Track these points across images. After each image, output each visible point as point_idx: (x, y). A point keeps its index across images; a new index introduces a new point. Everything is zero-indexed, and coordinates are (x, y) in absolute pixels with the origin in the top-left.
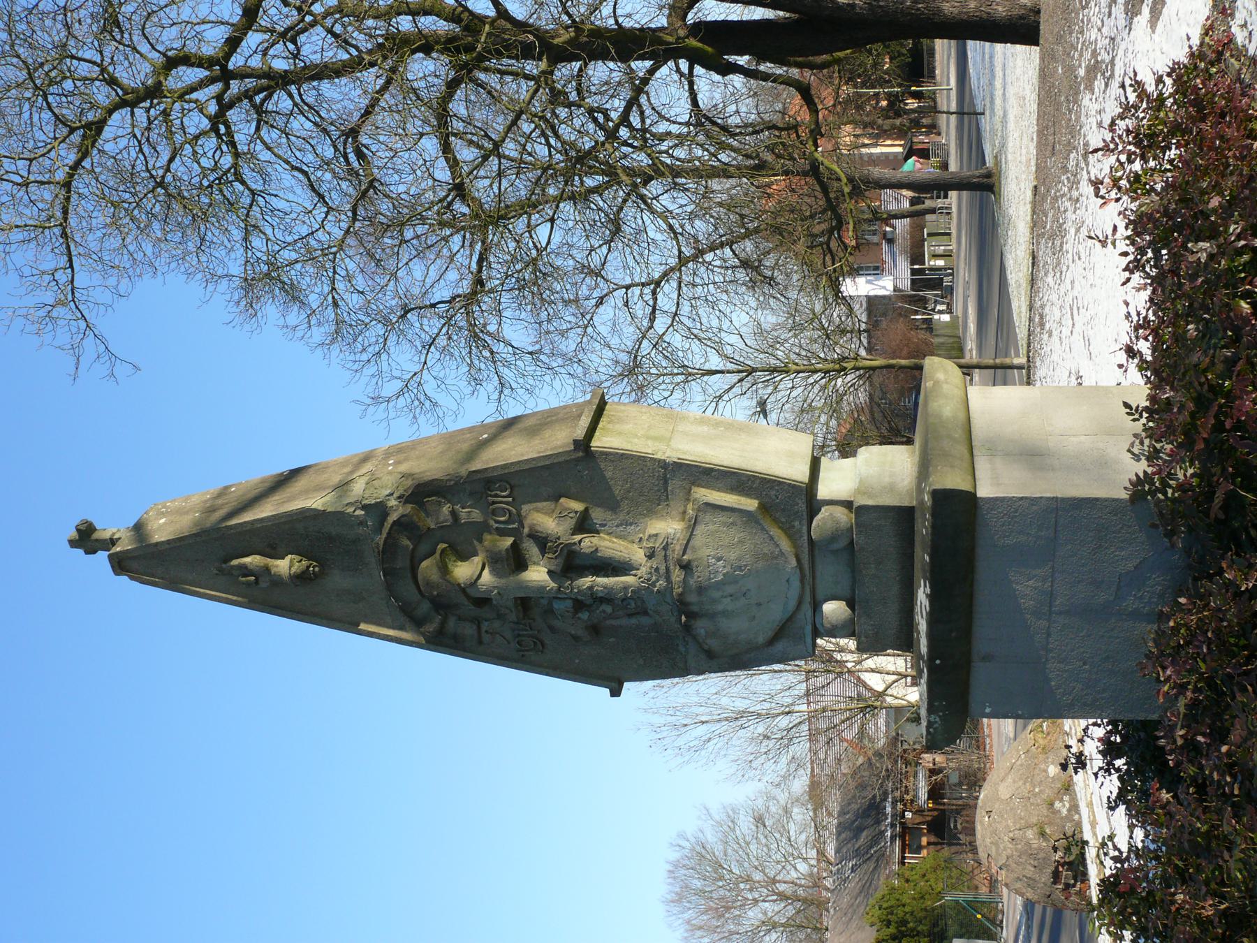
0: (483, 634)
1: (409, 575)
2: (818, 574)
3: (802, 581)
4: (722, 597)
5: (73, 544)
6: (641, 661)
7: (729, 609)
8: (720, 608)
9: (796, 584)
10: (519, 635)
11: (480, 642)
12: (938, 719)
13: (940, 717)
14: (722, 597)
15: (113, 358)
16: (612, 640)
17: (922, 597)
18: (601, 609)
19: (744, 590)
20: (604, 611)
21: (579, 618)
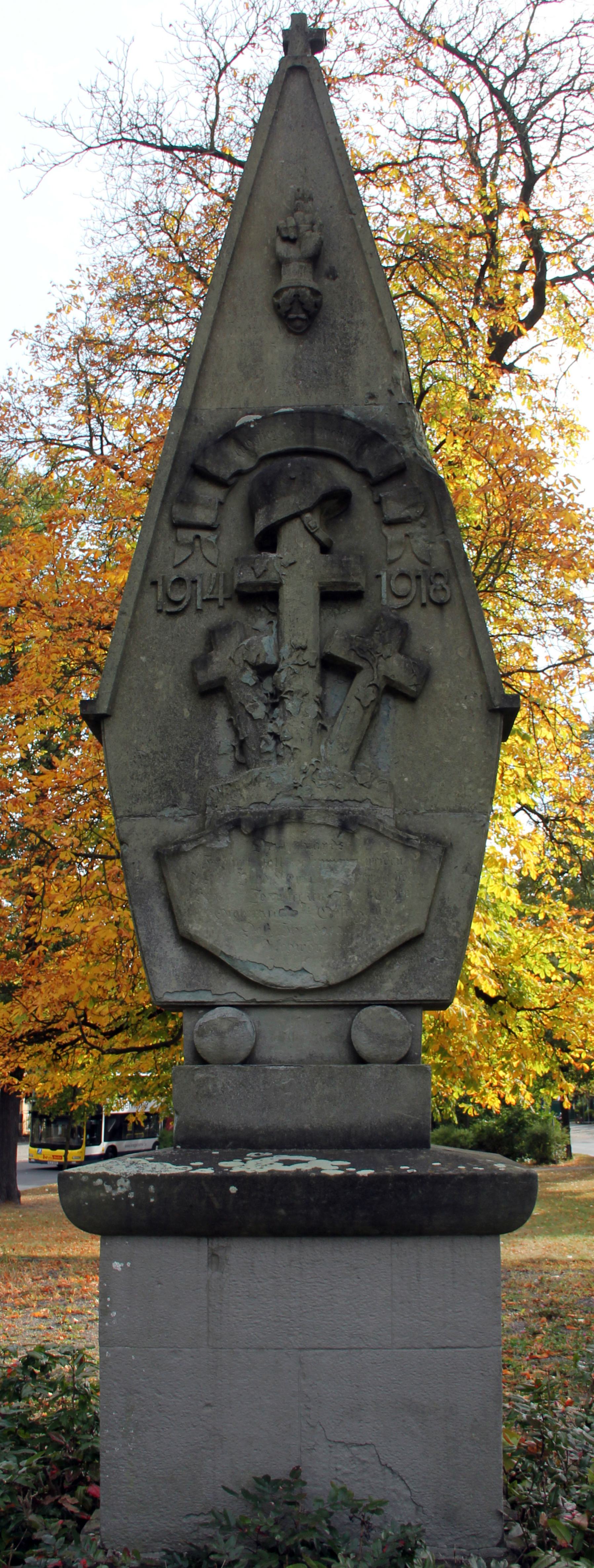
0: (194, 532)
1: (301, 446)
2: (298, 1013)
3: (301, 991)
4: (289, 877)
5: (299, 19)
6: (145, 750)
7: (266, 885)
8: (269, 871)
9: (297, 982)
10: (194, 582)
11: (177, 525)
12: (120, 1190)
13: (127, 1193)
14: (289, 877)
15: (46, 169)
16: (186, 713)
17: (330, 1168)
18: (259, 703)
19: (298, 908)
20: (255, 707)
21: (243, 670)
